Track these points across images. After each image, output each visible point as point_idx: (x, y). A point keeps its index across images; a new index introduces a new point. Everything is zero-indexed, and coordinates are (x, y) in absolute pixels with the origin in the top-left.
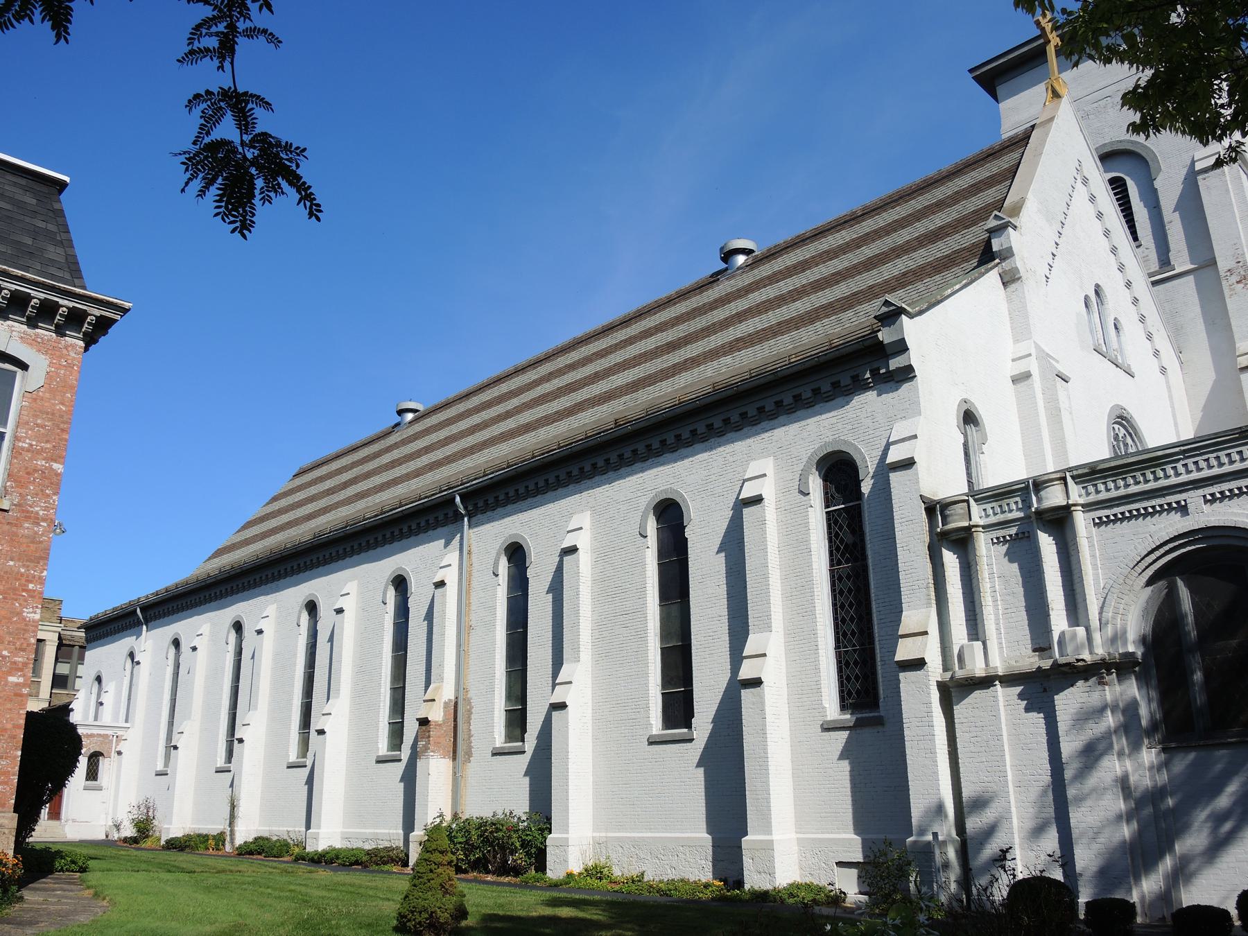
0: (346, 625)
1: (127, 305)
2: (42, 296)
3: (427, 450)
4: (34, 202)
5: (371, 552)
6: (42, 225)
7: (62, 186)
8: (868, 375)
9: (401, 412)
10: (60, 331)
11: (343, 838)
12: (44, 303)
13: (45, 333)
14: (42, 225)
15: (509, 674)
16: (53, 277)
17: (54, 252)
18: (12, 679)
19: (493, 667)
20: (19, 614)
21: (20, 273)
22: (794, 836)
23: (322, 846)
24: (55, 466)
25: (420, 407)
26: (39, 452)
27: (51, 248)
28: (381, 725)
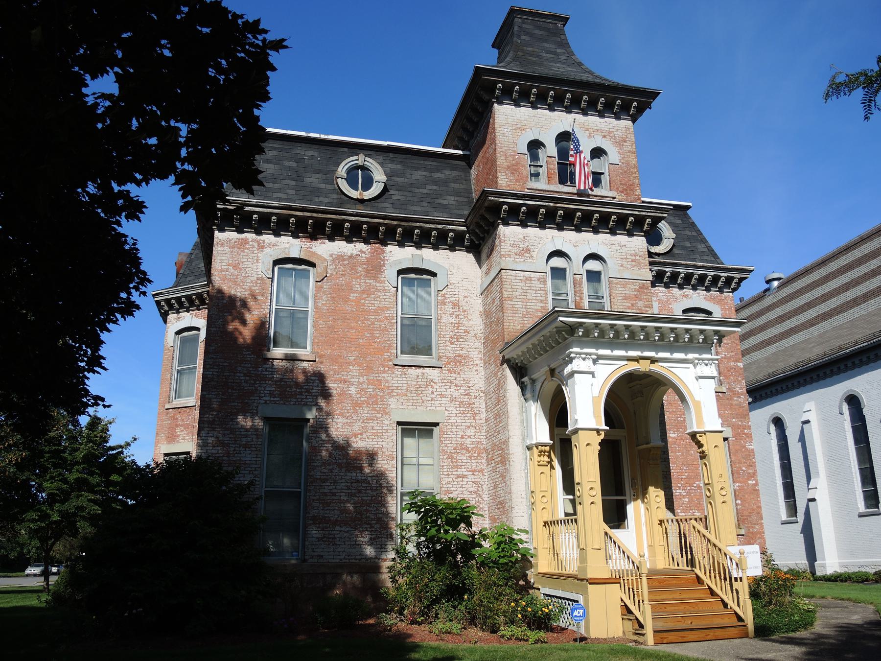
0: (814, 431)
1: (752, 268)
2: (712, 274)
3: (809, 305)
4: (680, 221)
5: (828, 380)
6: (689, 233)
7: (689, 207)
8: (185, 9)
9: (768, 282)
10: (721, 291)
11: (840, 566)
12: (727, 278)
13: (714, 293)
14: (689, 233)
15: (858, 450)
16: (707, 261)
17: (701, 247)
18: (750, 482)
19: (846, 447)
20: (745, 447)
21: (701, 264)
22: (837, 561)
23: (829, 571)
24: (739, 364)
25: (781, 276)
26: (730, 358)
27: (699, 245)
28: (857, 492)
